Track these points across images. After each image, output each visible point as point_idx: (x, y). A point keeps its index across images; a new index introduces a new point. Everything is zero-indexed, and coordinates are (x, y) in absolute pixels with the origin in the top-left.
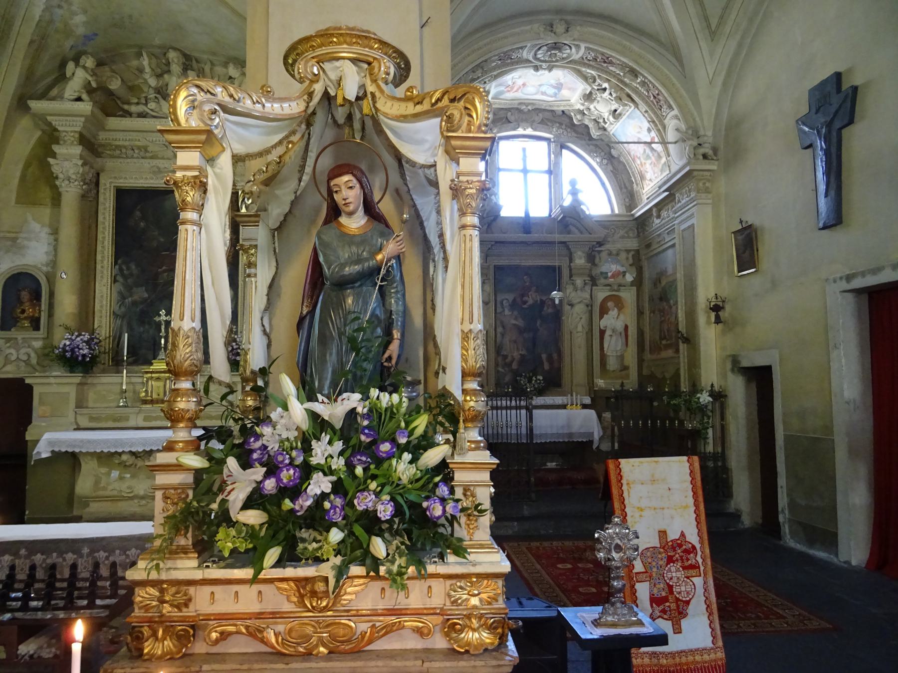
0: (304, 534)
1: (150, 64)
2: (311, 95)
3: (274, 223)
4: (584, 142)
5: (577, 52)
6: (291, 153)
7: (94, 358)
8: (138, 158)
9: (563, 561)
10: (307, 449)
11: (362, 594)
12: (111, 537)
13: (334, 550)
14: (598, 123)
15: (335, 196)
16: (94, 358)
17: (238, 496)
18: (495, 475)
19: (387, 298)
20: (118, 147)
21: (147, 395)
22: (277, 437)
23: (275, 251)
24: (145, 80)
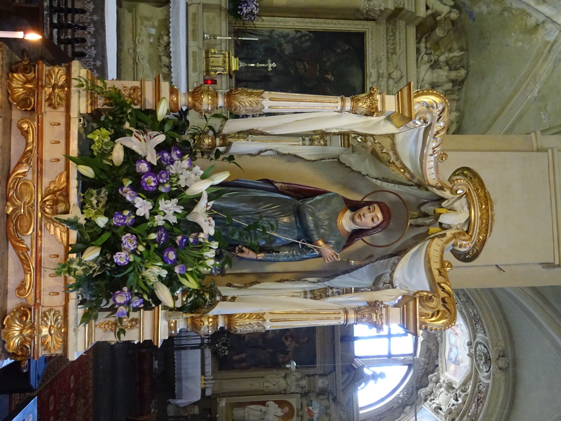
0: (104, 192)
1: (455, 56)
2: (441, 188)
3: (345, 158)
4: (414, 383)
5: (484, 377)
6: (397, 171)
7: (239, 17)
8: (387, 48)
9: (76, 381)
10: (170, 196)
11: (54, 240)
12: (105, 36)
13: (90, 218)
14: (430, 395)
15: (366, 208)
16: (239, 17)
17: (134, 143)
18: (148, 344)
19: (289, 248)
20: (394, 34)
21: (212, 54)
22: (180, 172)
23: (323, 159)
24: (444, 53)
